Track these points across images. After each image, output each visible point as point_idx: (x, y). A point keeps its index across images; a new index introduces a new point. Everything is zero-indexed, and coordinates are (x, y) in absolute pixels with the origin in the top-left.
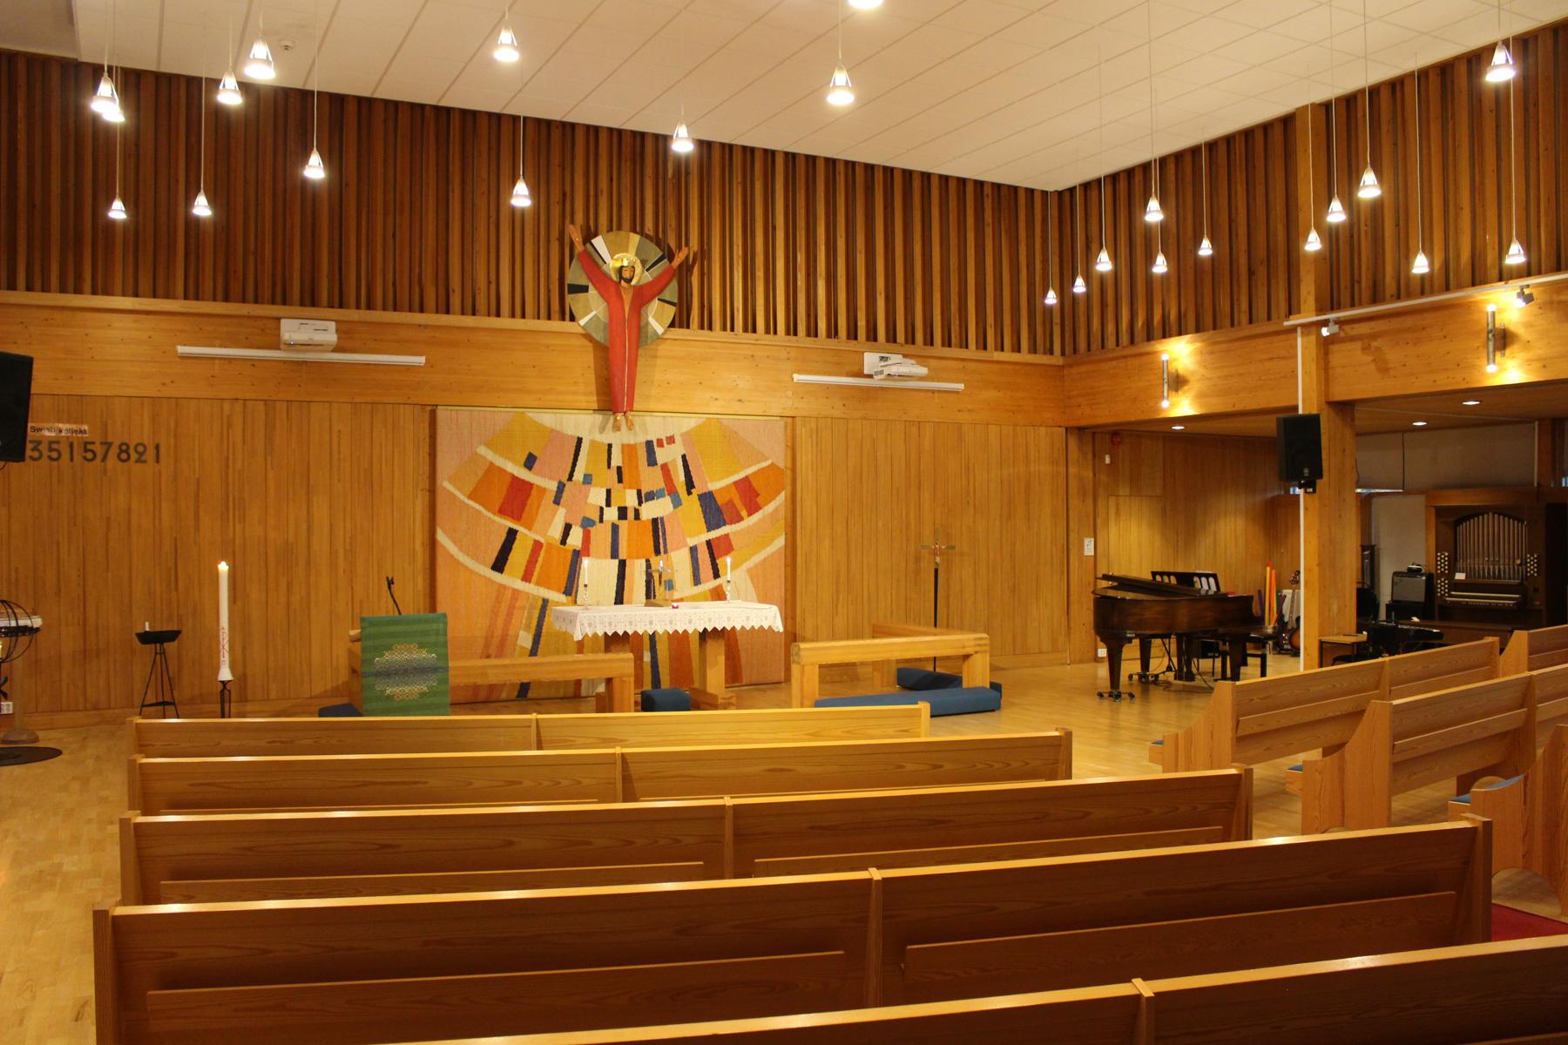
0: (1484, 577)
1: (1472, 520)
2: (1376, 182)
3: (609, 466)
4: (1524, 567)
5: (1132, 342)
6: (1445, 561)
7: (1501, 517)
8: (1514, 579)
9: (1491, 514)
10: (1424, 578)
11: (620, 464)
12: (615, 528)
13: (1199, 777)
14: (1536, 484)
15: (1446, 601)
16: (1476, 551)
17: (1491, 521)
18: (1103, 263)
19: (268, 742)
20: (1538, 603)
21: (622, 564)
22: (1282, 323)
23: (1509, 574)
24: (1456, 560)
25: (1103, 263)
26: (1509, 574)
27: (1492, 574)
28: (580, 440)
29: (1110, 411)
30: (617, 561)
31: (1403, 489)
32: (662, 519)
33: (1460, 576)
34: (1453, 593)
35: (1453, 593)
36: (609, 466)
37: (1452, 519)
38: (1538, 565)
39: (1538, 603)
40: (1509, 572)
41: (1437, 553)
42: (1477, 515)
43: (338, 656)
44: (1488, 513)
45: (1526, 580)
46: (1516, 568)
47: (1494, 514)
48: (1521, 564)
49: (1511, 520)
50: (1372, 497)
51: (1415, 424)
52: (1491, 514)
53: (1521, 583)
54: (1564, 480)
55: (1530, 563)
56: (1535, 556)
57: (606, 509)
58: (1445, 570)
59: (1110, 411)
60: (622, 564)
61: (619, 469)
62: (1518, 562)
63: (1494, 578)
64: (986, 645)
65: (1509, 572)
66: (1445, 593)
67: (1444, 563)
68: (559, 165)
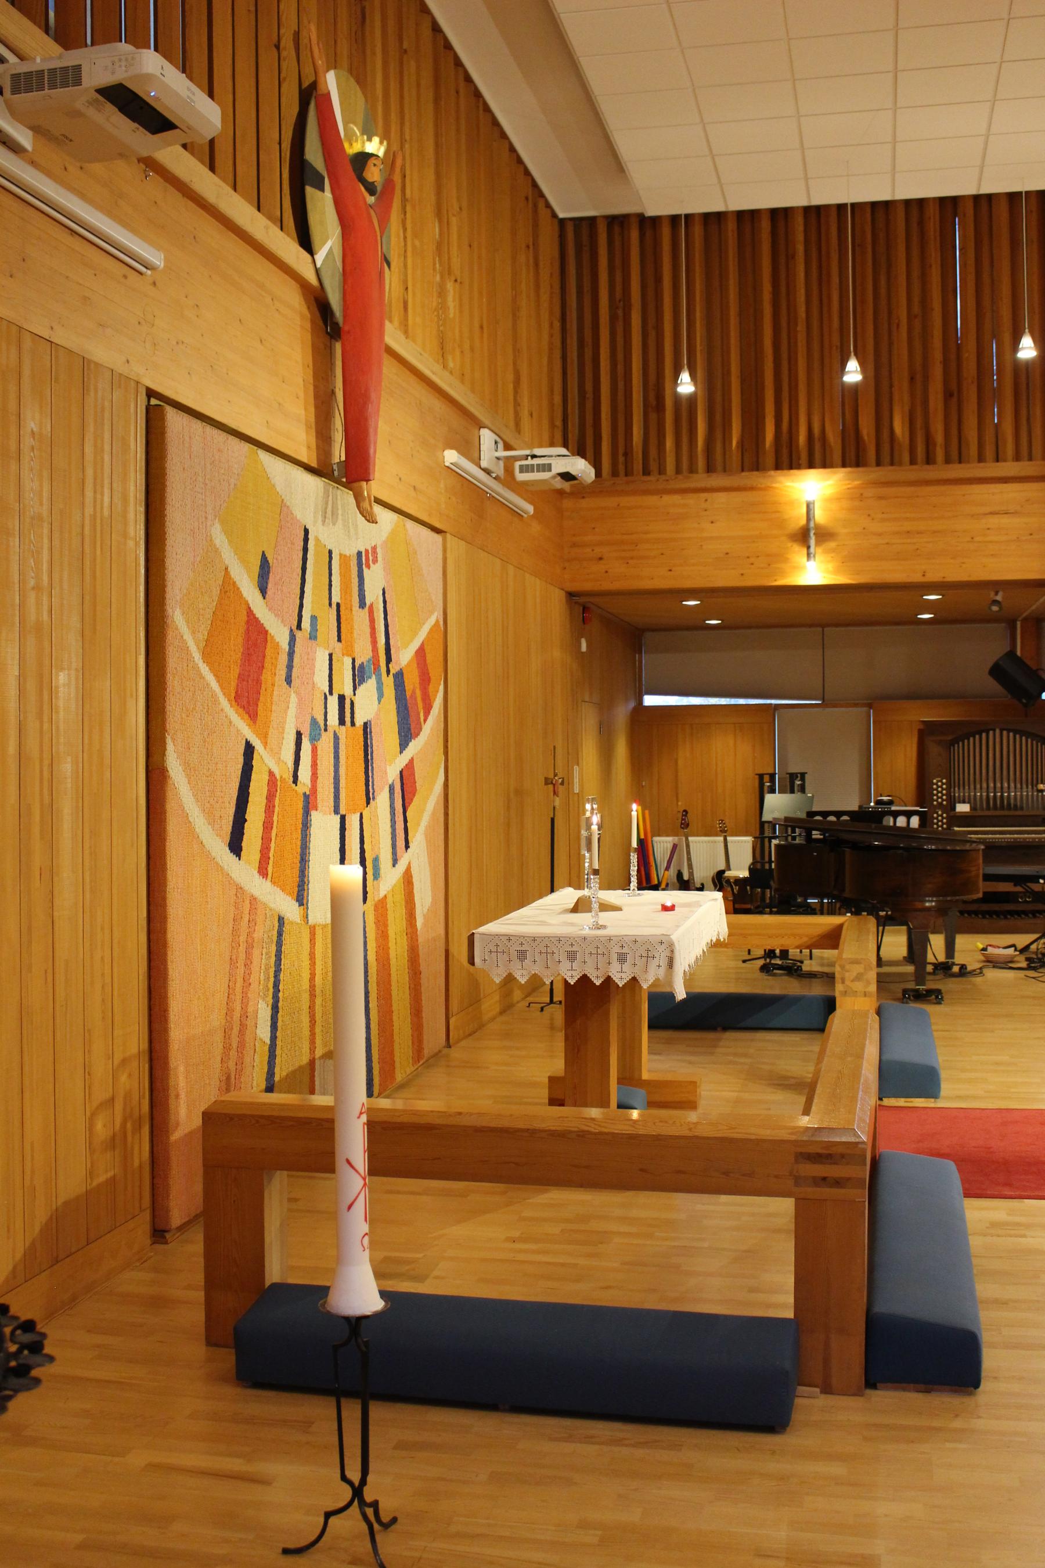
0: (982, 809)
2: (859, 369)
3: (330, 605)
5: (678, 471)
6: (943, 789)
9: (998, 731)
11: (339, 601)
12: (336, 738)
16: (984, 771)
17: (998, 740)
18: (685, 383)
19: (264, 1481)
21: (343, 819)
25: (685, 383)
27: (1030, 806)
28: (330, 552)
29: (593, 550)
30: (339, 816)
32: (370, 721)
33: (963, 808)
36: (330, 605)
43: (32, 1144)
44: (994, 730)
51: (919, 616)
52: (998, 731)
57: (329, 697)
58: (943, 800)
59: (593, 550)
60: (343, 819)
61: (338, 605)
63: (995, 808)
68: (406, 141)
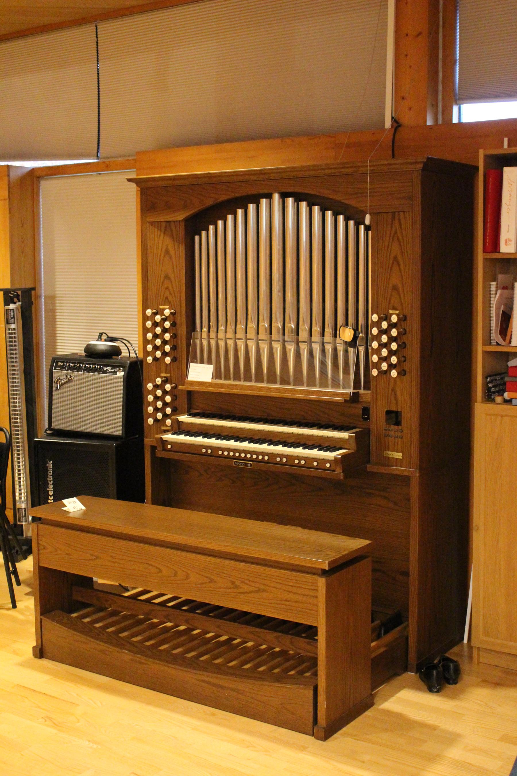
1: (240, 212)
4: (362, 349)
7: (304, 205)
8: (336, 383)
9: (276, 197)
10: (121, 374)
13: (385, 75)
14: (388, 124)
15: (164, 443)
20: (399, 455)
22: (370, 646)
23: (324, 372)
24: (192, 327)
26: (324, 372)
31: (98, 157)
34: (184, 418)
35: (184, 418)
37: (181, 216)
38: (402, 346)
39: (399, 455)
40: (323, 363)
41: (145, 307)
42: (256, 199)
44: (269, 196)
45: (367, 387)
46: (340, 348)
47: (284, 196)
48: (353, 343)
49: (329, 214)
50: (39, 178)
52: (276, 197)
53: (355, 398)
54: (455, 109)
55: (378, 338)
56: (394, 319)
62: (347, 334)
64: (136, 311)
65: (323, 363)
66: (166, 416)
67: (162, 410)
